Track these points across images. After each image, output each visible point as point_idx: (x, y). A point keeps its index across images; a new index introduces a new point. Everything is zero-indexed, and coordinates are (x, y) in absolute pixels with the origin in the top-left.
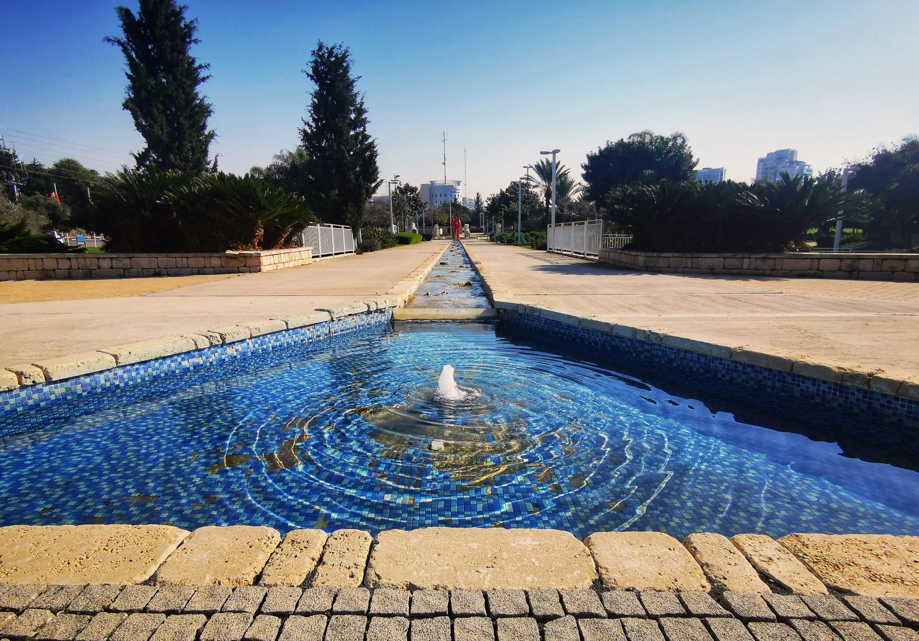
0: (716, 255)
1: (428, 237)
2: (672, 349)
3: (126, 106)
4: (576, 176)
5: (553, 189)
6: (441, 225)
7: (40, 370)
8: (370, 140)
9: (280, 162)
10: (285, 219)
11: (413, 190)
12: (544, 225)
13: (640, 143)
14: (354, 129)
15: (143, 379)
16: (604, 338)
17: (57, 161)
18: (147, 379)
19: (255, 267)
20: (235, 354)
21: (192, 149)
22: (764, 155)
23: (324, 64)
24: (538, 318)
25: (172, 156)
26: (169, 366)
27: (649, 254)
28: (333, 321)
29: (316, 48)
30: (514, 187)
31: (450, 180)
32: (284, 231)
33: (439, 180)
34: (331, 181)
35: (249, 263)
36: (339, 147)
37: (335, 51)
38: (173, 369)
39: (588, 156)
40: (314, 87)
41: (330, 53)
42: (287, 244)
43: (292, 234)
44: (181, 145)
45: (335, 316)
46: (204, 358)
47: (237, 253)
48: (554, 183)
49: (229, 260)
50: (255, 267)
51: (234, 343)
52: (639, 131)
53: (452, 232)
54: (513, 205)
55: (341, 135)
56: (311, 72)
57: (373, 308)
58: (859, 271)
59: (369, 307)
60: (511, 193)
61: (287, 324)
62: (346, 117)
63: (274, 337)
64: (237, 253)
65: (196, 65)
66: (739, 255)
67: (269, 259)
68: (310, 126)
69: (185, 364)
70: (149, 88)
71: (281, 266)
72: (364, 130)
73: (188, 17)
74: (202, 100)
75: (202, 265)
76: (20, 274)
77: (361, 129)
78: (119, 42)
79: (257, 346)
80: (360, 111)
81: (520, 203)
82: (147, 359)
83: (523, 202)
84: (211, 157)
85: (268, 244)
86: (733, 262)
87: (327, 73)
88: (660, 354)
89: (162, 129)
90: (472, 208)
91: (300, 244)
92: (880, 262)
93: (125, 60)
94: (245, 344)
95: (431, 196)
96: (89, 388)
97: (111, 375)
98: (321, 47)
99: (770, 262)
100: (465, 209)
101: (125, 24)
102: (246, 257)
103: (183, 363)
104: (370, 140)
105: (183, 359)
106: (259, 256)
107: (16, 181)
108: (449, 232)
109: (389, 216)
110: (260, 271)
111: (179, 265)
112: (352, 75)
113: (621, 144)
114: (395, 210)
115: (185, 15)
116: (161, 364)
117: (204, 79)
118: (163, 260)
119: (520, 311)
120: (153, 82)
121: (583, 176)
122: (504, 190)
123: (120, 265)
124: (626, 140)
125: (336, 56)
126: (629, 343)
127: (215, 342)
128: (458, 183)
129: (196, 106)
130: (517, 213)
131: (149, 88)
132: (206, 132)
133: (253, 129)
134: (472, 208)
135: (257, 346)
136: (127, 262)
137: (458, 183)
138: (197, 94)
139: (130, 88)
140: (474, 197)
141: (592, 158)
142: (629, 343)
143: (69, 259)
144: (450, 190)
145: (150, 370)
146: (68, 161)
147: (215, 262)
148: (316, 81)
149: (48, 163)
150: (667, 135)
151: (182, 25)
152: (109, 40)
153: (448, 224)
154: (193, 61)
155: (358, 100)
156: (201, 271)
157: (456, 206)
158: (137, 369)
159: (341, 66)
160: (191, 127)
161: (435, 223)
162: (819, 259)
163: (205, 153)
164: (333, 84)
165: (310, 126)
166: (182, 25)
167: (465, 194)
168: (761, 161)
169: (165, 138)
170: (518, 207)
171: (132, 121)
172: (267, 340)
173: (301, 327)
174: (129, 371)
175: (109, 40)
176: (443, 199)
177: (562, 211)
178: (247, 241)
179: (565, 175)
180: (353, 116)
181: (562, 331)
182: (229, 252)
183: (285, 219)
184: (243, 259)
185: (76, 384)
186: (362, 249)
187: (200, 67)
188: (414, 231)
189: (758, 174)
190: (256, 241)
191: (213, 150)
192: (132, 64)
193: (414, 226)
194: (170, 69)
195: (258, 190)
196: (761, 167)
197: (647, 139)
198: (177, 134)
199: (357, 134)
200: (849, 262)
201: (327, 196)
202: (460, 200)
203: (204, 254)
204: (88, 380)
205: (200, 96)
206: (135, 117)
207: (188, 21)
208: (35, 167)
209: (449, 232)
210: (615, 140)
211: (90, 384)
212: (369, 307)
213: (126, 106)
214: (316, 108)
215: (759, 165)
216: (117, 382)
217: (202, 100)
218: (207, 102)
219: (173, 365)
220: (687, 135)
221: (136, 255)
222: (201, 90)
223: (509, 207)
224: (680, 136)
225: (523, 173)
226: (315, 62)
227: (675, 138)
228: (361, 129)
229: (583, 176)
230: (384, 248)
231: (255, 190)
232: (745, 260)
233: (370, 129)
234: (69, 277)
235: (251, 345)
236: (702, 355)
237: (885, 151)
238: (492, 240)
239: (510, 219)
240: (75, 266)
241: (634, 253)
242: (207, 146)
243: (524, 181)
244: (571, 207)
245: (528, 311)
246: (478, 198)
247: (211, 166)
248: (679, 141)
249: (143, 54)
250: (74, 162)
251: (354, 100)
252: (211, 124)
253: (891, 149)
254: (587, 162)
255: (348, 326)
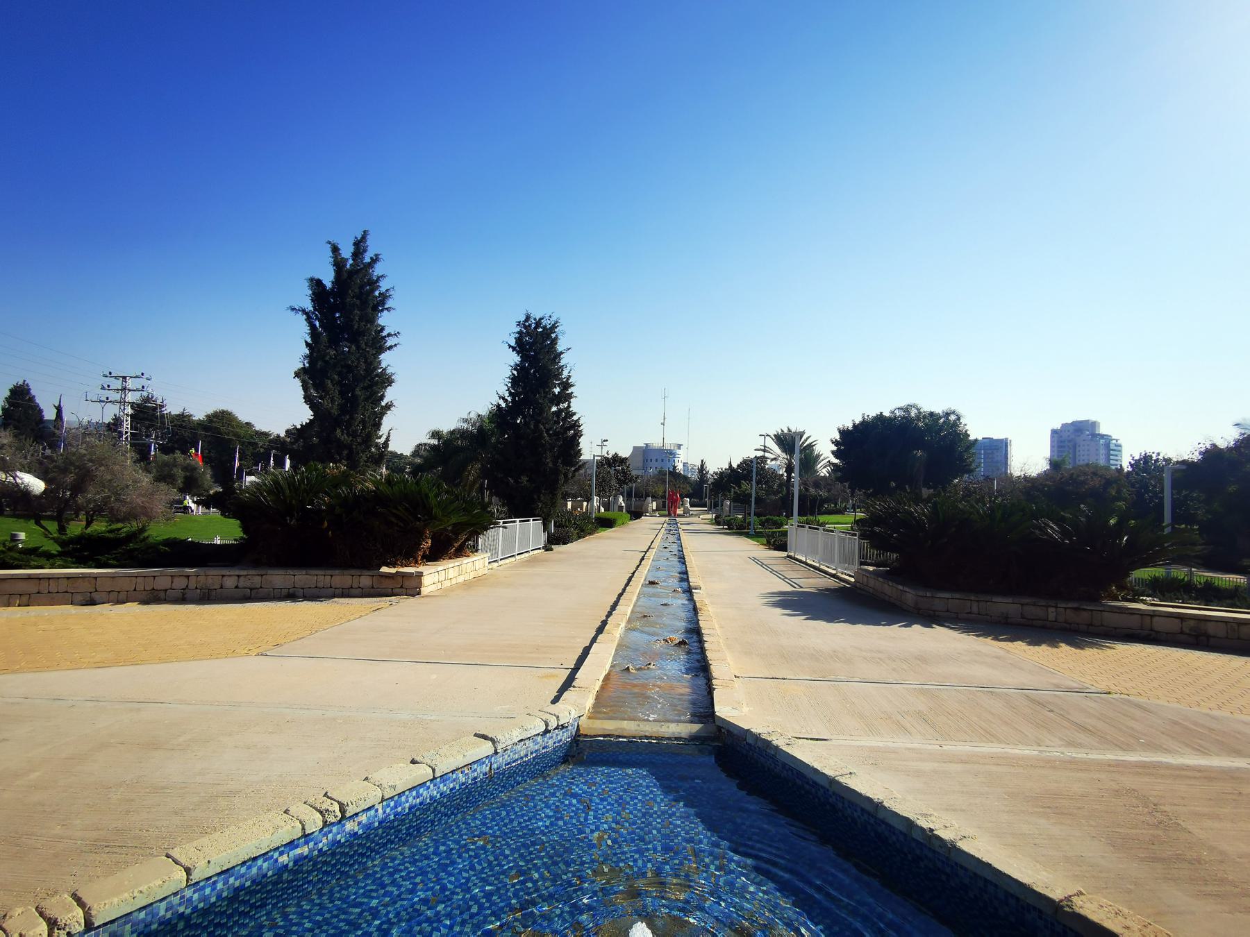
0: (1010, 600)
1: (636, 514)
2: (966, 870)
3: (297, 374)
4: (825, 450)
5: (795, 463)
6: (654, 497)
7: (80, 912)
8: (575, 418)
9: (465, 426)
10: (458, 528)
11: (623, 461)
12: (784, 506)
13: (903, 418)
14: (557, 405)
15: (219, 897)
16: (866, 817)
17: (210, 411)
18: (225, 894)
19: (410, 587)
20: (356, 829)
21: (363, 421)
22: (1058, 426)
23: (528, 334)
24: (773, 758)
25: (338, 431)
26: (260, 868)
27: (921, 593)
28: (496, 753)
29: (523, 319)
30: (747, 463)
31: (669, 443)
32: (456, 540)
33: (656, 442)
34: (525, 461)
35: (407, 584)
36: (536, 426)
37: (544, 322)
38: (265, 871)
39: (839, 430)
40: (516, 358)
41: (538, 324)
42: (459, 553)
43: (467, 539)
44: (352, 418)
45: (500, 748)
46: (311, 844)
47: (393, 570)
48: (797, 456)
49: (383, 580)
50: (410, 587)
51: (357, 814)
52: (903, 404)
53: (668, 507)
54: (744, 485)
55: (541, 410)
56: (513, 343)
57: (553, 724)
58: (1208, 637)
59: (547, 725)
60: (743, 469)
61: (434, 771)
62: (550, 391)
63: (414, 793)
64: (393, 570)
65: (385, 333)
66: (1042, 602)
67: (435, 576)
68: (506, 401)
69: (284, 859)
70: (327, 358)
71: (447, 584)
72: (569, 406)
73: (384, 286)
74: (384, 369)
75: (348, 584)
76: (123, 596)
77: (566, 405)
78: (304, 312)
79: (388, 810)
80: (566, 385)
81: (754, 483)
82: (230, 866)
83: (758, 483)
84: (384, 431)
85: (435, 556)
86: (1035, 609)
87: (531, 345)
88: (948, 870)
89: (333, 401)
90: (694, 476)
91: (475, 550)
92: (1235, 626)
93: (307, 329)
94: (372, 812)
95: (645, 461)
96: (141, 926)
97: (176, 900)
98: (528, 318)
99: (1085, 615)
100: (686, 478)
101: (314, 293)
102: (404, 575)
103: (280, 860)
104: (575, 418)
105: (281, 854)
106: (420, 575)
107: (157, 437)
108: (664, 506)
109: (590, 486)
110: (419, 593)
111: (320, 585)
112: (560, 347)
113: (880, 418)
114: (599, 485)
115: (381, 284)
116: (249, 868)
117: (390, 348)
118: (301, 578)
119: (750, 740)
120: (332, 352)
121: (833, 452)
122: (735, 465)
123: (248, 584)
124: (887, 414)
125: (544, 328)
126: (901, 838)
127: (331, 819)
128: (679, 446)
129: (377, 375)
130: (750, 495)
131: (327, 358)
132: (383, 404)
133: (436, 390)
134: (694, 476)
135: (388, 810)
136: (257, 580)
137: (679, 446)
138: (380, 363)
139: (306, 357)
140: (699, 464)
141: (843, 433)
142: (901, 838)
143: (188, 577)
144: (670, 454)
145: (232, 880)
146: (223, 412)
147: (365, 581)
148: (518, 353)
149: (199, 412)
150: (939, 410)
151: (377, 293)
152: (293, 309)
153: (664, 497)
154: (383, 329)
155: (565, 373)
156: (346, 593)
157: (674, 474)
158: (215, 883)
159: (548, 336)
160: (366, 399)
161: (647, 496)
162: (1152, 616)
163: (378, 425)
164: (537, 352)
165: (506, 401)
166: (377, 293)
167: (687, 460)
168: (1054, 432)
169: (335, 412)
170: (751, 488)
171: (301, 393)
172: (403, 799)
173: (453, 772)
174: (203, 888)
175: (293, 309)
176: (659, 465)
177: (807, 490)
178: (409, 556)
179: (811, 446)
180: (557, 390)
181: (807, 787)
182: (384, 569)
183: (458, 528)
184: (400, 579)
185: (126, 923)
186: (554, 540)
187: (389, 335)
188: (621, 508)
189: (1052, 451)
190: (420, 553)
191: (387, 422)
192: (314, 332)
193: (621, 499)
194: (355, 337)
195: (431, 495)
196: (1056, 439)
197: (913, 413)
198: (350, 405)
199: (560, 411)
200: (1192, 623)
201: (516, 481)
202: (680, 467)
203: (353, 572)
204: (142, 915)
205: (383, 365)
206: (305, 388)
207: (383, 290)
208: (183, 419)
209: (664, 506)
210: (872, 413)
211: (143, 920)
212: (547, 725)
213: (297, 374)
214: (515, 381)
215: (1052, 437)
216: (181, 909)
217: (384, 369)
218: (389, 371)
219: (265, 865)
220: (960, 410)
221: (270, 572)
222: (386, 359)
223: (740, 487)
224: (953, 412)
225: (759, 443)
226: (520, 333)
227: (947, 414)
228: (566, 405)
229: (833, 452)
230: (580, 537)
231: (427, 496)
232: (1051, 610)
233: (575, 405)
234: (183, 599)
235: (380, 811)
236: (1012, 896)
237: (1214, 445)
238: (717, 522)
239: (742, 500)
240: (192, 585)
241: (900, 587)
242: (381, 418)
243: (760, 454)
244: (819, 483)
245: (759, 744)
246: (702, 466)
247: (382, 440)
248: (952, 418)
249: (328, 323)
250: (230, 414)
251: (561, 374)
252: (390, 394)
253: (1222, 444)
254: (838, 437)
255: (516, 756)
